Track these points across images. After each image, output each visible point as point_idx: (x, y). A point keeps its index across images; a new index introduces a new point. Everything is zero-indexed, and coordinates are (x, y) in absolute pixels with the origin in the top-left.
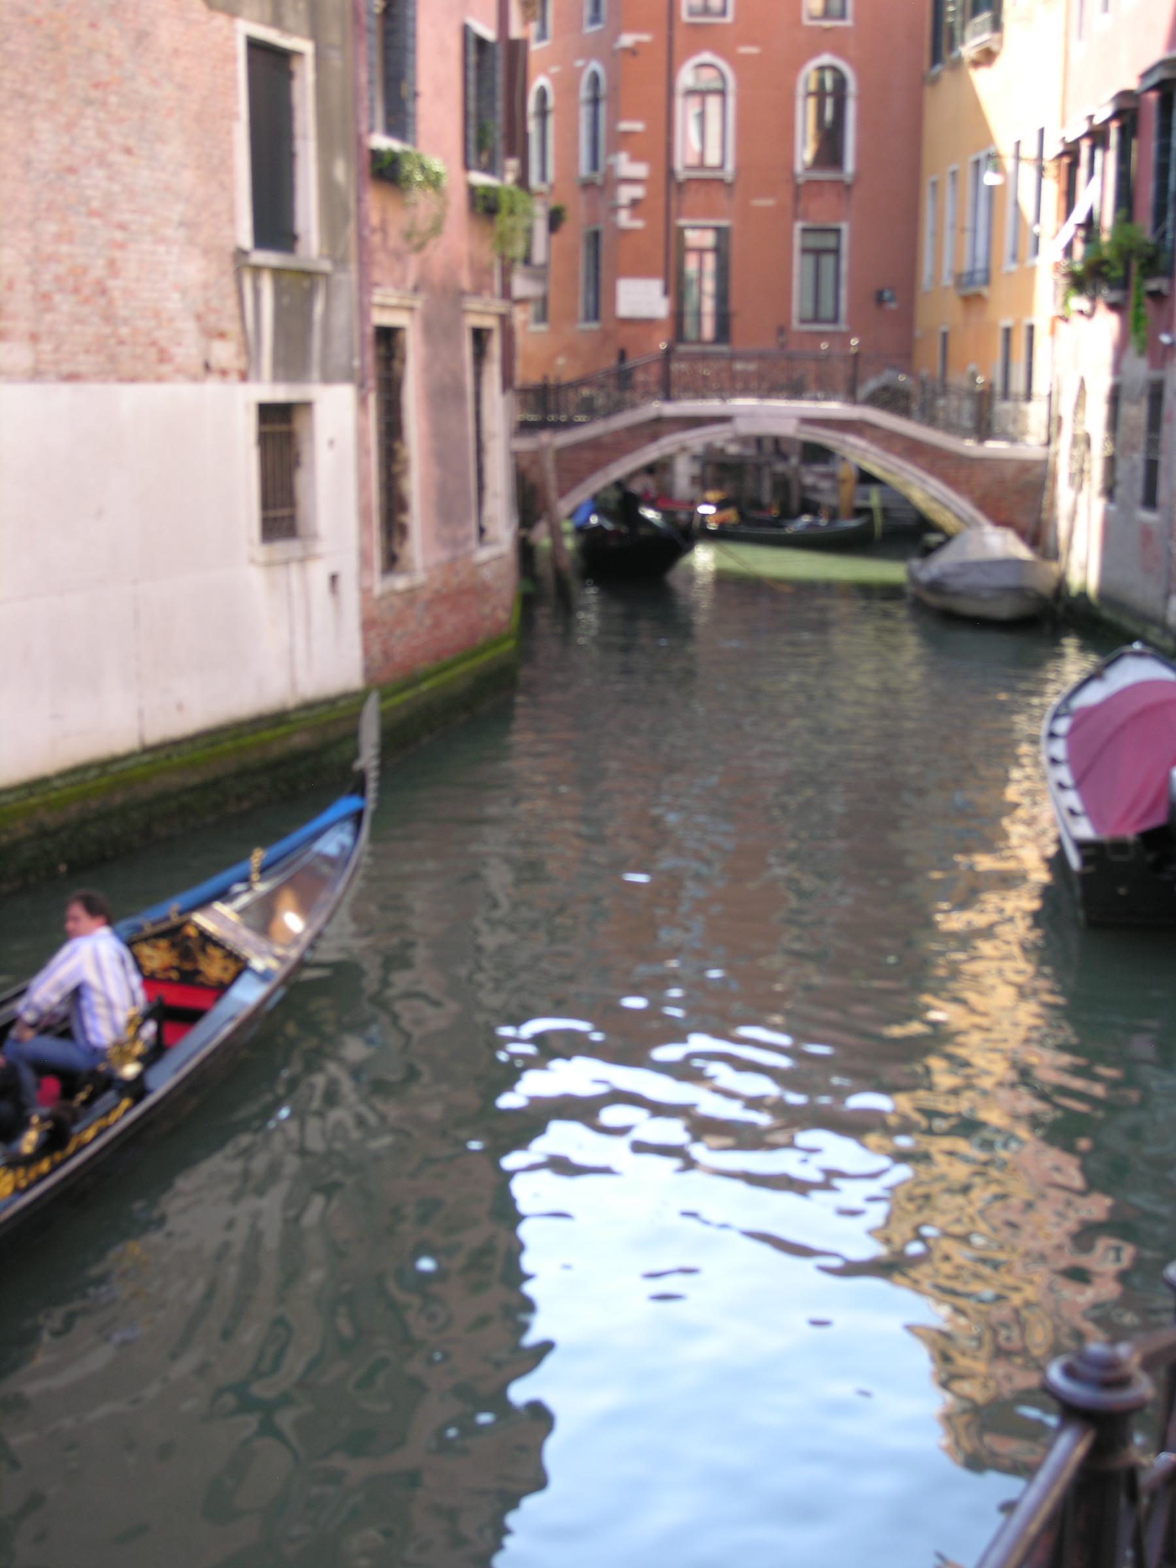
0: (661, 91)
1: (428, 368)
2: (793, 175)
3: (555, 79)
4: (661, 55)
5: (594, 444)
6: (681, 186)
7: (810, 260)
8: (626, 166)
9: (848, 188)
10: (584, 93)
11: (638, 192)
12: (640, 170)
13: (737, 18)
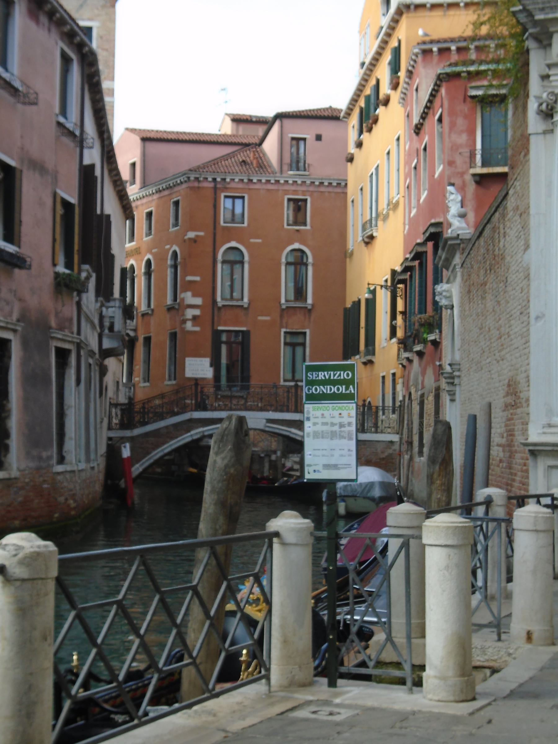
0: (210, 261)
1: (24, 363)
2: (280, 305)
3: (154, 255)
4: (210, 241)
5: (156, 433)
6: (219, 308)
7: (289, 349)
8: (189, 298)
9: (310, 311)
10: (169, 262)
11: (197, 312)
12: (198, 301)
13: (249, 225)
